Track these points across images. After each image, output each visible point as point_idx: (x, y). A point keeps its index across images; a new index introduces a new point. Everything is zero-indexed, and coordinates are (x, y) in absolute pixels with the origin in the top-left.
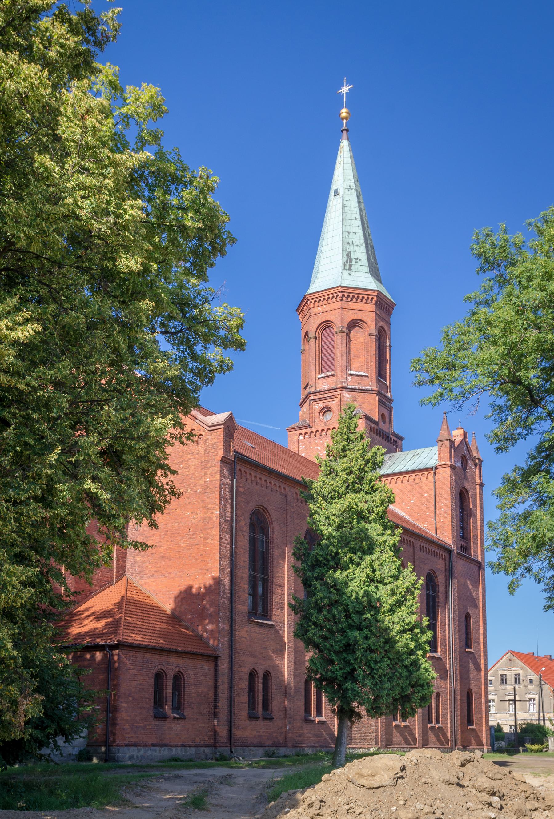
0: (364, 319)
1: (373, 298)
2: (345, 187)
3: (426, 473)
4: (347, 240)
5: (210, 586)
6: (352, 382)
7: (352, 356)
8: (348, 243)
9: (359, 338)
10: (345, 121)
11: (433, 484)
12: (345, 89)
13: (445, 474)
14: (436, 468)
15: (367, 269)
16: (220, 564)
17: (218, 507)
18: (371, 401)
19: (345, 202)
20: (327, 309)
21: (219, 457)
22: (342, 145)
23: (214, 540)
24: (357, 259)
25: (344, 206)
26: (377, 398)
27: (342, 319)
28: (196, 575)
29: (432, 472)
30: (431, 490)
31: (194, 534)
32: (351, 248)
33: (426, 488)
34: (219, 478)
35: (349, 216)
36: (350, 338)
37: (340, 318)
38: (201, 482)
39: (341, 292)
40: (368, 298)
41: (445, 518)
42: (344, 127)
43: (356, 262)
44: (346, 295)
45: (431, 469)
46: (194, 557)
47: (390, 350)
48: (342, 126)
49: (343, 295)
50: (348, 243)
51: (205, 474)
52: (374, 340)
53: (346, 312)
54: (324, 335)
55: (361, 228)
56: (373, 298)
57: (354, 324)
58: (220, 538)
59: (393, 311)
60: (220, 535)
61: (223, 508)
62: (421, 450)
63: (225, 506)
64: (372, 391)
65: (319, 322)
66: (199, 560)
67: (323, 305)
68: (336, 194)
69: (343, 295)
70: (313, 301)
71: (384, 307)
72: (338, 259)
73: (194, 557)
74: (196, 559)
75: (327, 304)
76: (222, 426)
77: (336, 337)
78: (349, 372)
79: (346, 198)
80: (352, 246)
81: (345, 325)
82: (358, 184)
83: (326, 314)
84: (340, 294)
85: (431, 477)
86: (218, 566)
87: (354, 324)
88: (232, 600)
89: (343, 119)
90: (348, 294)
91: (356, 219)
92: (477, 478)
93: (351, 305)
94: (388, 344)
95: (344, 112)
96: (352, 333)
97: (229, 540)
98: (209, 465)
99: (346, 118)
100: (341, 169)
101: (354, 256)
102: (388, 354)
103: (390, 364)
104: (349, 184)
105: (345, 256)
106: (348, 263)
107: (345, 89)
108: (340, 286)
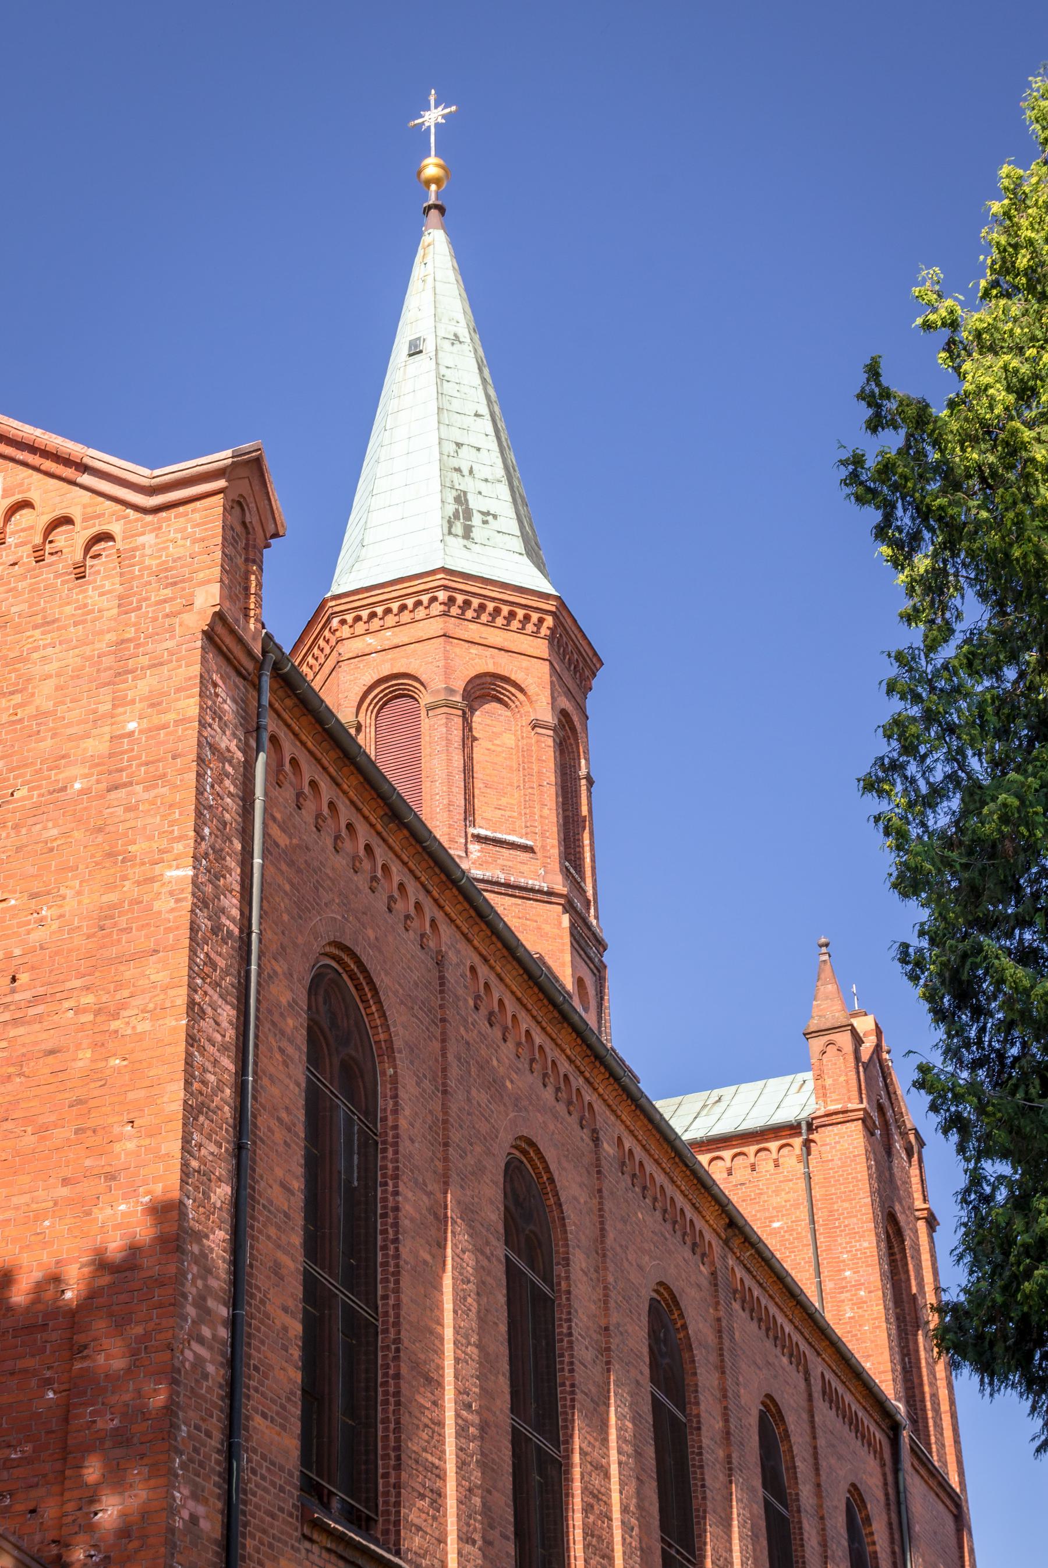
0: (517, 676)
1: (541, 620)
2: (441, 333)
3: (773, 1145)
4: (455, 463)
5: (134, 1250)
6: (481, 864)
7: (478, 784)
8: (458, 470)
9: (497, 735)
10: (433, 187)
11: (802, 1184)
12: (433, 117)
13: (846, 1146)
14: (809, 1125)
15: (518, 545)
16: (186, 1140)
17: (185, 847)
18: (547, 928)
19: (443, 371)
20: (397, 641)
21: (198, 619)
22: (426, 239)
23: (156, 1013)
24: (488, 514)
25: (441, 379)
26: (566, 920)
27: (447, 667)
28: (39, 1217)
29: (797, 1142)
30: (796, 1206)
31: (37, 1000)
32: (467, 484)
33: (776, 1200)
34: (194, 711)
35: (456, 405)
36: (471, 730)
37: (439, 661)
38: (96, 746)
39: (446, 588)
40: (527, 618)
41: (860, 1303)
42: (432, 200)
43: (485, 522)
44: (460, 598)
45: (792, 1129)
46: (28, 1120)
47: (589, 791)
48: (426, 197)
49: (452, 600)
50: (458, 470)
51: (119, 702)
52: (550, 742)
53: (459, 650)
54: (384, 722)
55: (493, 437)
56: (541, 620)
57: (485, 690)
58: (191, 1004)
59: (594, 683)
60: (192, 988)
61: (208, 862)
62: (727, 1091)
63: (219, 855)
64: (550, 893)
65: (369, 679)
66: (60, 1134)
67: (383, 628)
68: (415, 351)
69: (452, 600)
70: (349, 618)
71: (575, 660)
72: (433, 509)
73: (28, 1120)
74: (42, 1130)
75: (398, 625)
76: (221, 483)
77: (425, 723)
78: (471, 830)
79: (446, 359)
80: (468, 479)
81: (459, 685)
82: (476, 337)
83: (390, 655)
84: (442, 596)
85: (791, 1159)
86: (175, 1146)
87: (485, 690)
88: (234, 1361)
89: (428, 183)
90: (463, 597)
91: (477, 415)
92: (917, 1195)
93: (473, 631)
94: (583, 772)
95: (431, 167)
96: (478, 718)
97: (231, 1033)
98: (144, 661)
99: (437, 181)
100: (429, 295)
101: (475, 503)
102: (584, 800)
103: (591, 834)
104: (453, 329)
105: (451, 500)
106: (461, 518)
107: (433, 117)
108: (443, 570)
